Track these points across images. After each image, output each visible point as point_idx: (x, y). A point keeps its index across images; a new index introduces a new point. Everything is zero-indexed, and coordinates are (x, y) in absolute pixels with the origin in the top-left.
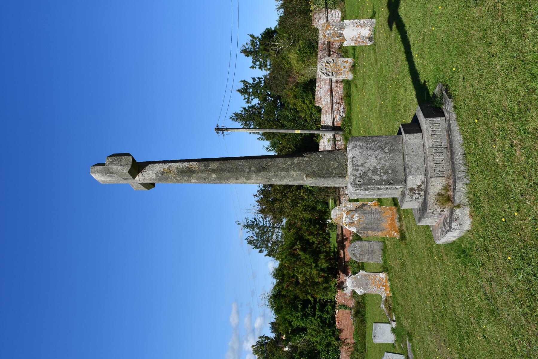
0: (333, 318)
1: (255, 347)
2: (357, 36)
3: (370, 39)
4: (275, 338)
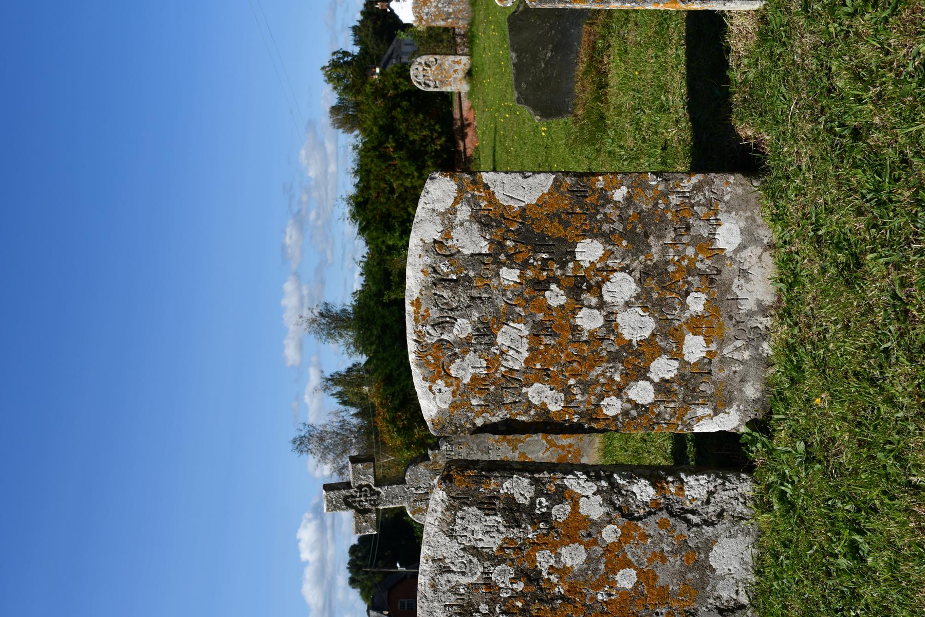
1: (327, 69)
4: (360, 53)
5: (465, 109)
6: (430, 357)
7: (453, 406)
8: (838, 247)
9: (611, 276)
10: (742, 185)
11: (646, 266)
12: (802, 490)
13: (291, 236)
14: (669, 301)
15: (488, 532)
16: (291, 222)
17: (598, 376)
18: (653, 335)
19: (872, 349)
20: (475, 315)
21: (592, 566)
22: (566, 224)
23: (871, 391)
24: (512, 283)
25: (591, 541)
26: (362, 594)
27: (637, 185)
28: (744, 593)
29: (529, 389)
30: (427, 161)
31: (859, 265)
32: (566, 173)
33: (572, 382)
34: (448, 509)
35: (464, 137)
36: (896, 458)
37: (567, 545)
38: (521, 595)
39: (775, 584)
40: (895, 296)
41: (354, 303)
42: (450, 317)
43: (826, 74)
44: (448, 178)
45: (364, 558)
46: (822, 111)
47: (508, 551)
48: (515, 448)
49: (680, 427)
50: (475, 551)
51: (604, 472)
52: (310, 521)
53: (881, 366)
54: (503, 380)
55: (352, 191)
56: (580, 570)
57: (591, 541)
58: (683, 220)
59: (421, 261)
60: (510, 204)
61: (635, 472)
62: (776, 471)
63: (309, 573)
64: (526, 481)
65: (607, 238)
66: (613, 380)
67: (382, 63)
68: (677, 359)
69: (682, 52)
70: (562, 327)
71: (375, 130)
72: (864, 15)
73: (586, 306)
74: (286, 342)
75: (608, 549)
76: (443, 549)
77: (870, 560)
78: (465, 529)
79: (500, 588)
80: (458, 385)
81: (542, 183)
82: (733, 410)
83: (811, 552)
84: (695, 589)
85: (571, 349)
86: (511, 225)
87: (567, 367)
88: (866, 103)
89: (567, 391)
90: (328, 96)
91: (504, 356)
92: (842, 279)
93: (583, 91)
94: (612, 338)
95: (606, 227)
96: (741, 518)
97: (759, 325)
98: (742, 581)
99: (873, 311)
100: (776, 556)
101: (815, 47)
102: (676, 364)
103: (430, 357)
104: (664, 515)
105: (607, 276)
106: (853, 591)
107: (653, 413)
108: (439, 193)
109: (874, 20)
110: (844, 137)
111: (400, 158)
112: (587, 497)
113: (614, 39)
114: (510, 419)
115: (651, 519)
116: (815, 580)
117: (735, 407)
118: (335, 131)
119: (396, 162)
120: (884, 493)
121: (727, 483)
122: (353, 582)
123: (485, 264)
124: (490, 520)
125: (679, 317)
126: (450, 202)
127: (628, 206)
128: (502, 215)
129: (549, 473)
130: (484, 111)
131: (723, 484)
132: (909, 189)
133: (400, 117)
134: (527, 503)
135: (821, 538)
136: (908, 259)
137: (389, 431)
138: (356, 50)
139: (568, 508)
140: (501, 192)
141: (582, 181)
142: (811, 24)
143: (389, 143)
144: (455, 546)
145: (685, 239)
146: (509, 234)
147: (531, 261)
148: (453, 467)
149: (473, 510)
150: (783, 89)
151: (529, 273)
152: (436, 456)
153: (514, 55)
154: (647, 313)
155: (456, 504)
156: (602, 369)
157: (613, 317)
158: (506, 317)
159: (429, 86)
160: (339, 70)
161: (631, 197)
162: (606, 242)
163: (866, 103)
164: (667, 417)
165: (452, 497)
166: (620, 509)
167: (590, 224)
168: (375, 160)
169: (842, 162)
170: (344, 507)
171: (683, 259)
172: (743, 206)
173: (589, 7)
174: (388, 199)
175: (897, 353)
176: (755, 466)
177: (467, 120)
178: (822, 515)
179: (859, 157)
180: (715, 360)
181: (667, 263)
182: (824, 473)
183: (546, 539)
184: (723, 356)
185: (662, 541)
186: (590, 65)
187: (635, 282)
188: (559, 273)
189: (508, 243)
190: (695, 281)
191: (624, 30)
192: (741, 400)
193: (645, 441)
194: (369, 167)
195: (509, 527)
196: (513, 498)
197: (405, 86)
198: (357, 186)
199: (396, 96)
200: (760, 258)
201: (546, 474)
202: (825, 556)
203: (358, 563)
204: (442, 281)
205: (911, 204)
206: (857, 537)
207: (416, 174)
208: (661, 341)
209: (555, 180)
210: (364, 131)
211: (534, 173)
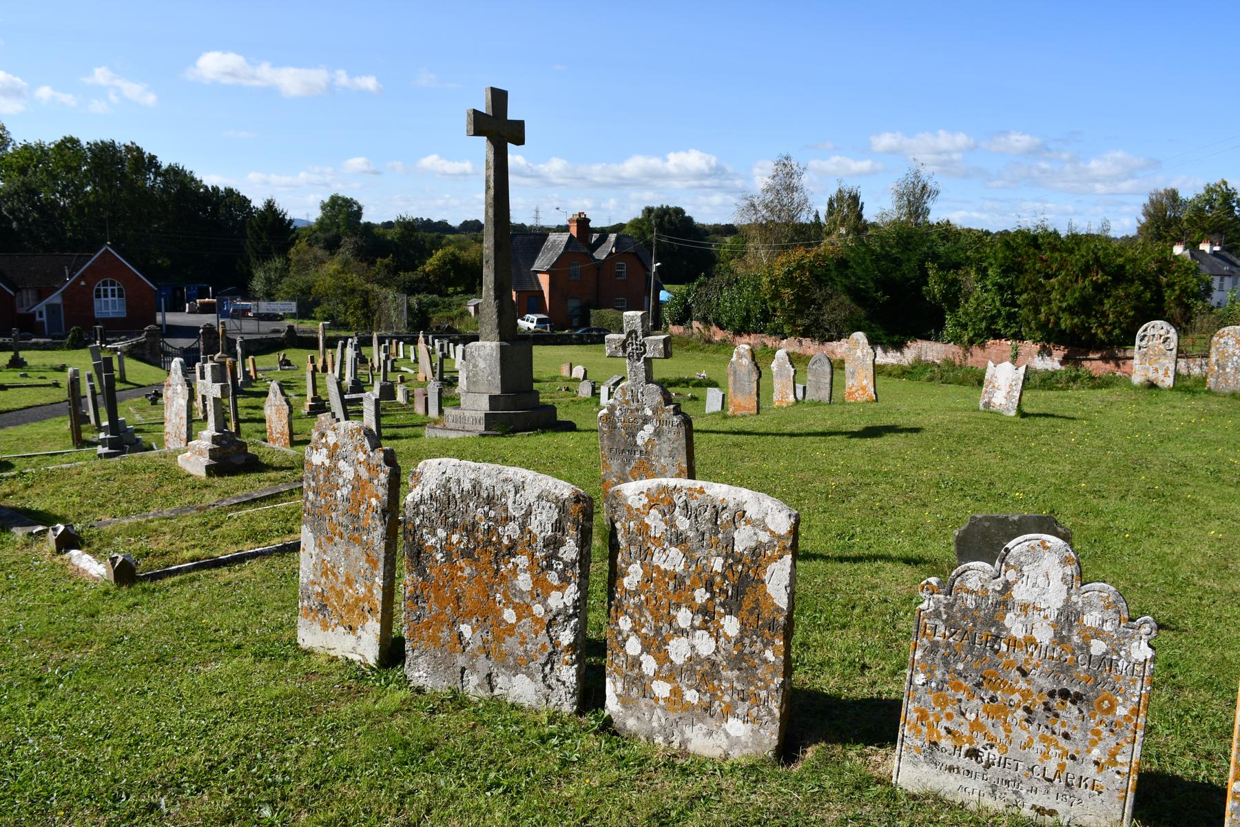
0: (998, 336)
1: (1224, 187)
2: (996, 385)
3: (987, 405)
6: (663, 495)
7: (629, 508)
13: (1020, 141)
16: (1037, 141)
18: (672, 662)
20: (691, 534)
21: (517, 594)
22: (751, 612)
25: (535, 596)
30: (1079, 317)
33: (643, 598)
34: (556, 497)
38: (501, 543)
50: (528, 514)
52: (708, 163)
63: (655, 163)
65: (739, 641)
67: (1225, 253)
71: (1120, 261)
80: (643, 513)
85: (664, 601)
89: (636, 593)
95: (747, 641)
102: (652, 674)
103: (663, 495)
104: (550, 649)
108: (779, 520)
111: (1085, 287)
115: (547, 640)
119: (1080, 282)
126: (772, 528)
128: (760, 566)
133: (1132, 290)
143: (1102, 276)
144: (532, 499)
145: (735, 696)
149: (556, 516)
151: (718, 579)
152: (669, 412)
159: (1141, 340)
160: (1221, 200)
164: (617, 661)
166: (554, 619)
171: (722, 692)
174: (1039, 272)
177: (1124, 364)
180: (652, 702)
181: (720, 680)
183: (535, 564)
188: (717, 601)
190: (707, 698)
194: (1077, 253)
199: (1159, 285)
201: (578, 571)
206: (501, 790)
207: (1064, 305)
209: (782, 609)
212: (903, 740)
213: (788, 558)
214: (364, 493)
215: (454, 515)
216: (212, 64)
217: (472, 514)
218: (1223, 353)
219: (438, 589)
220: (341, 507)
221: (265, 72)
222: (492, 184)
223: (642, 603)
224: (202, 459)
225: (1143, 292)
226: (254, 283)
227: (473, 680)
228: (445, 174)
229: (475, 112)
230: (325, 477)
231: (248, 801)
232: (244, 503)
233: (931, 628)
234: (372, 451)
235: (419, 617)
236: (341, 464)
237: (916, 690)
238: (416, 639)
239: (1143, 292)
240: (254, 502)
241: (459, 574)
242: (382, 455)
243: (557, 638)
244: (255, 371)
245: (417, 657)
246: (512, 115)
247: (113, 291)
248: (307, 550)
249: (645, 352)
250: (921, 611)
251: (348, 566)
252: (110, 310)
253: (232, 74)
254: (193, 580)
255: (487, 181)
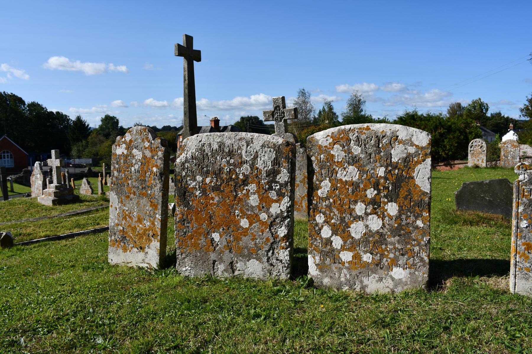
4: (487, 117)
5: (459, 166)
6: (343, 135)
7: (320, 147)
8: (392, 319)
9: (380, 219)
10: (423, 280)
11: (385, 235)
12: (282, 299)
13: (397, 86)
14: (368, 245)
15: (264, 163)
16: (403, 86)
17: (334, 212)
18: (353, 238)
19: (345, 329)
20: (362, 156)
21: (250, 208)
22: (405, 198)
23: (326, 328)
24: (377, 173)
25: (261, 208)
26: (238, 122)
27: (424, 232)
28: (239, 273)
29: (328, 181)
31: (384, 327)
32: (430, 198)
33: (331, 200)
34: (274, 144)
35: (446, 165)
36: (297, 335)
37: (259, 198)
38: (237, 178)
39: (243, 286)
40: (369, 340)
41: (366, 115)
42: (361, 144)
43: (477, 318)
44: (428, 142)
45: (253, 123)
46: (458, 315)
47: (256, 171)
48: (301, 182)
49: (310, 249)
51: (291, 214)
52: (268, 99)
53: (337, 332)
54: (332, 169)
55: (419, 113)
56: (248, 203)
57: (261, 208)
58: (407, 253)
59: (388, 130)
60: (416, 172)
61: (291, 228)
62: (291, 289)
63: (245, 99)
64: (286, 179)
65: (398, 217)
66: (332, 219)
67: (482, 127)
68: (341, 248)
69: (488, 257)
70: (357, 196)
71: (449, 124)
72: (506, 334)
73: (366, 207)
74: (347, 85)
75: (257, 215)
76: (257, 143)
77: (254, 321)
78: (265, 152)
79: (240, 168)
80: (330, 148)
81: (425, 187)
82: (318, 272)
83: (256, 300)
84: (240, 253)
85: (346, 200)
86: (405, 172)
87: (338, 198)
88: (462, 333)
89: (327, 198)
90: (466, 102)
91: (343, 169)
92: (378, 319)
93: (469, 214)
94: (352, 219)
95: (404, 217)
96: (270, 274)
97: (356, 286)
98: (244, 273)
99: (362, 331)
100: (254, 287)
101: (490, 314)
102: (339, 248)
103: (343, 135)
105: (381, 217)
106: (241, 314)
107: (317, 237)
108: (421, 138)
109: (503, 338)
110: (445, 323)
111: (436, 135)
112: (280, 206)
113: (495, 229)
114: (314, 172)
115: (270, 235)
116: (244, 300)
117: (319, 273)
118: (449, 105)
120: (282, 329)
121: (285, 268)
122: (242, 118)
123: (387, 160)
124: (269, 164)
125: (360, 250)
126: (417, 143)
127: (414, 227)
128: (410, 168)
129: (290, 190)
130: (458, 173)
131: (285, 267)
132: (419, 348)
133: (456, 135)
134: (277, 180)
135: (262, 304)
136: (387, 345)
137: (308, 132)
138: (489, 115)
139: (275, 198)
140: (421, 167)
141: (426, 205)
142: (502, 312)
143: (443, 130)
144: (258, 148)
145: (397, 253)
146: (401, 171)
147: (388, 182)
148: (293, 147)
149: (274, 156)
150: (469, 299)
151: (382, 181)
153: (488, 182)
154: (363, 235)
155: (276, 148)
156: (337, 214)
157: (361, 219)
158: (362, 170)
159: (471, 148)
160: (479, 107)
161: (418, 229)
162: (397, 217)
163: (462, 333)
164: (315, 243)
165: (279, 146)
166: (274, 221)
167: (405, 209)
168: (434, 124)
169: (433, 322)
170: (275, 106)
171: (388, 252)
172: (413, 280)
173: (514, 210)
175: (343, 339)
176: (293, 281)
177: (454, 167)
178: (272, 305)
179: (435, 329)
180: (341, 265)
181: (386, 245)
182: (290, 307)
184: (342, 269)
185: (261, 239)
186: (482, 218)
187: (377, 230)
188: (382, 195)
189: (397, 171)
190: (378, 257)
191: (499, 233)
192: (322, 276)
193: (304, 238)
194: (431, 121)
195: (266, 172)
196: (279, 174)
197: (471, 137)
198: (422, 115)
199: (466, 133)
200: (388, 287)
201: (290, 188)
202: (255, 305)
203: (251, 121)
204: (379, 140)
205: (413, 348)
208: (350, 241)
209: (427, 193)
210: (449, 118)
211: (430, 183)
212: (516, 265)
213: (429, 161)
214: (149, 165)
215: (207, 166)
216: (54, 61)
217: (219, 164)
218: (506, 151)
219: (198, 213)
220: (134, 177)
221: (78, 65)
222: (187, 78)
223: (331, 204)
224: (50, 198)
225: (460, 136)
226: (72, 152)
227: (221, 267)
228: (156, 106)
229: (178, 45)
230: (124, 161)
231: (86, 335)
232: (73, 215)
233: (527, 191)
234: (153, 140)
235: (185, 233)
236: (135, 151)
237: (522, 231)
238: (184, 247)
239: (460, 136)
240: (78, 214)
241: (211, 202)
242: (160, 141)
243: (277, 233)
244: (74, 186)
245: (184, 258)
246: (195, 48)
247: (8, 156)
248: (114, 206)
249: (284, 116)
250: (519, 181)
251: (139, 211)
252: (7, 164)
253: (63, 66)
254: (45, 245)
255: (185, 77)
